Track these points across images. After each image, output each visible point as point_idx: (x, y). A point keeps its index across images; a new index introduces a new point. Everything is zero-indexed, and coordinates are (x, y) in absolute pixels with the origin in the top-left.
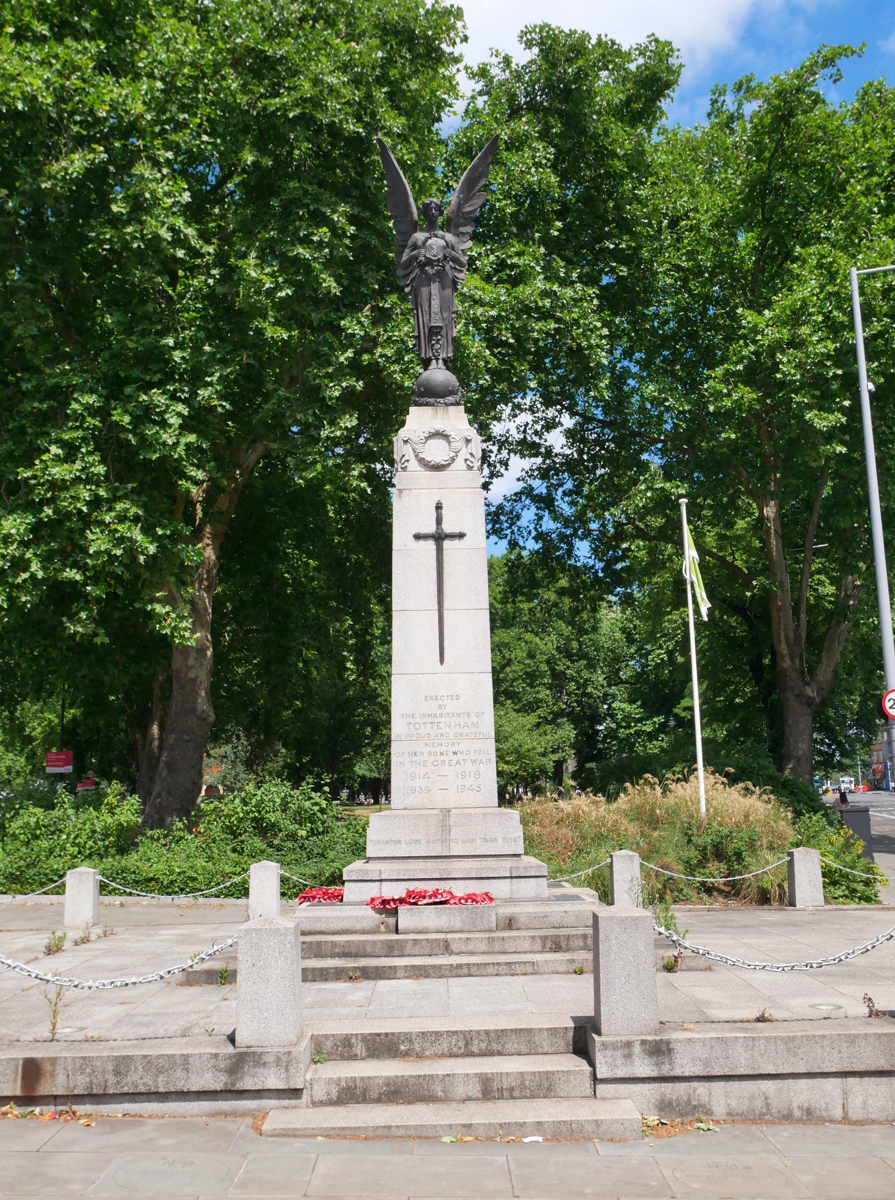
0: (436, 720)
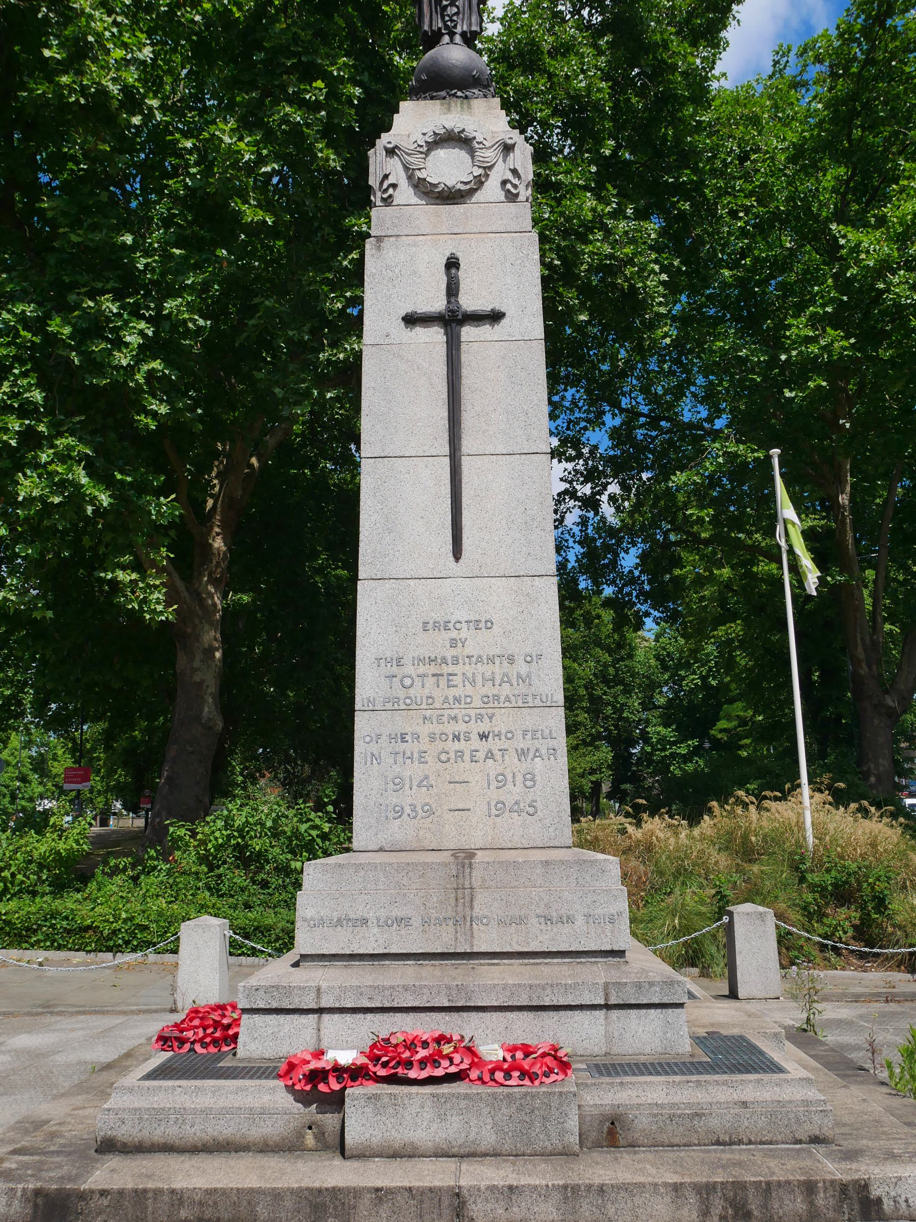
0: (446, 670)
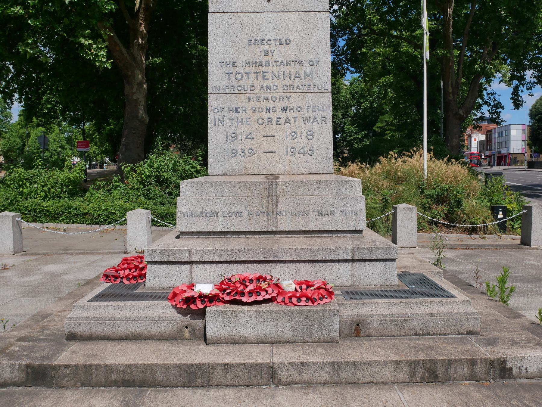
0: (262, 69)
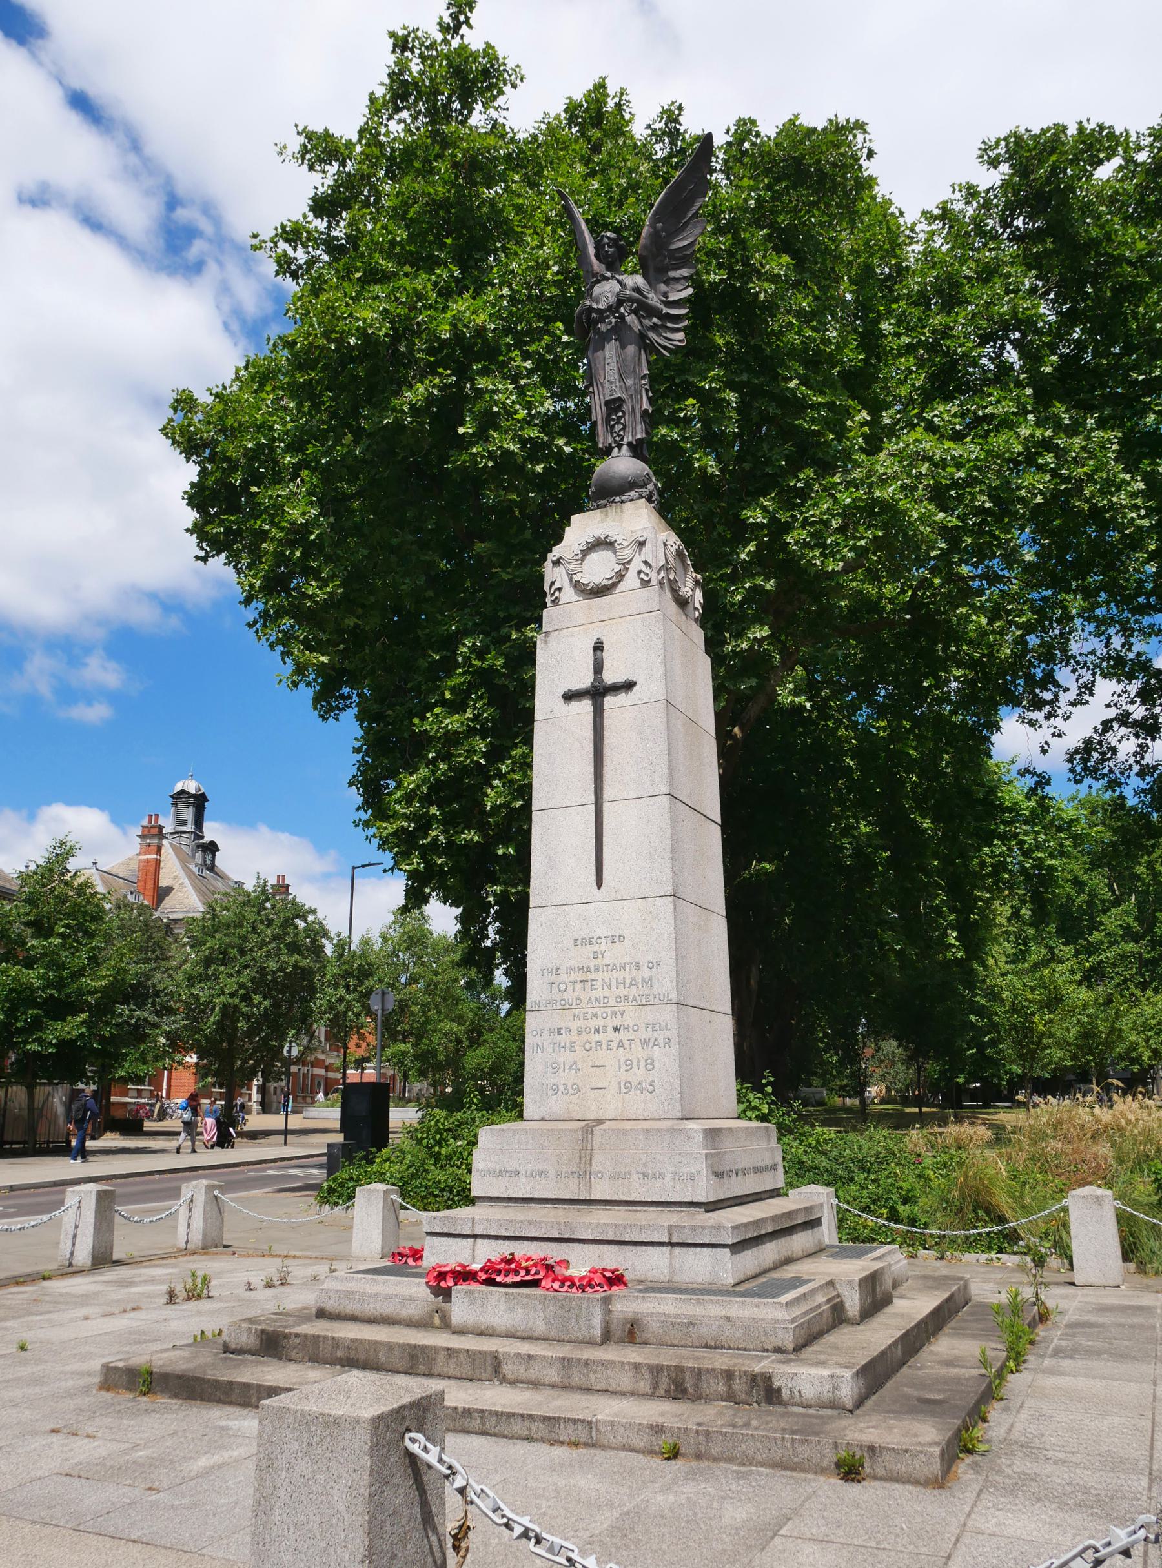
0: (590, 976)
